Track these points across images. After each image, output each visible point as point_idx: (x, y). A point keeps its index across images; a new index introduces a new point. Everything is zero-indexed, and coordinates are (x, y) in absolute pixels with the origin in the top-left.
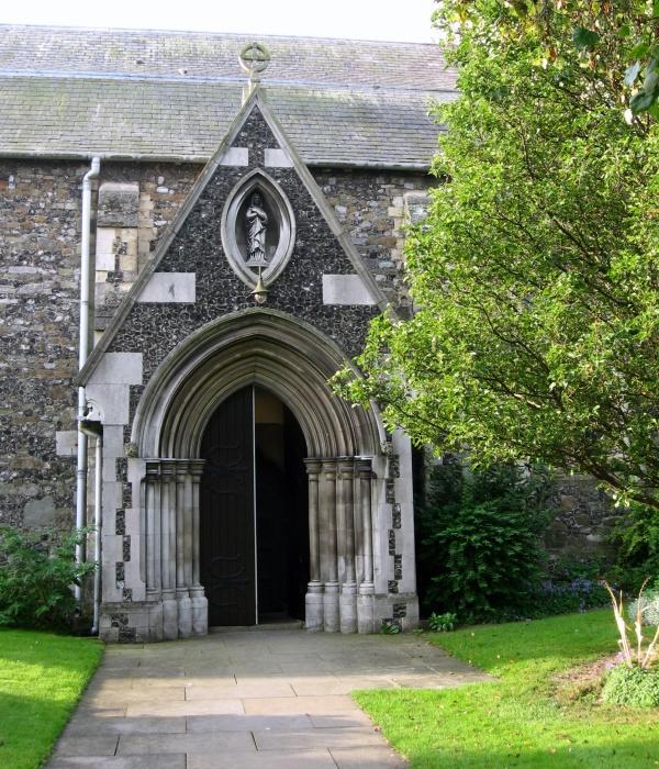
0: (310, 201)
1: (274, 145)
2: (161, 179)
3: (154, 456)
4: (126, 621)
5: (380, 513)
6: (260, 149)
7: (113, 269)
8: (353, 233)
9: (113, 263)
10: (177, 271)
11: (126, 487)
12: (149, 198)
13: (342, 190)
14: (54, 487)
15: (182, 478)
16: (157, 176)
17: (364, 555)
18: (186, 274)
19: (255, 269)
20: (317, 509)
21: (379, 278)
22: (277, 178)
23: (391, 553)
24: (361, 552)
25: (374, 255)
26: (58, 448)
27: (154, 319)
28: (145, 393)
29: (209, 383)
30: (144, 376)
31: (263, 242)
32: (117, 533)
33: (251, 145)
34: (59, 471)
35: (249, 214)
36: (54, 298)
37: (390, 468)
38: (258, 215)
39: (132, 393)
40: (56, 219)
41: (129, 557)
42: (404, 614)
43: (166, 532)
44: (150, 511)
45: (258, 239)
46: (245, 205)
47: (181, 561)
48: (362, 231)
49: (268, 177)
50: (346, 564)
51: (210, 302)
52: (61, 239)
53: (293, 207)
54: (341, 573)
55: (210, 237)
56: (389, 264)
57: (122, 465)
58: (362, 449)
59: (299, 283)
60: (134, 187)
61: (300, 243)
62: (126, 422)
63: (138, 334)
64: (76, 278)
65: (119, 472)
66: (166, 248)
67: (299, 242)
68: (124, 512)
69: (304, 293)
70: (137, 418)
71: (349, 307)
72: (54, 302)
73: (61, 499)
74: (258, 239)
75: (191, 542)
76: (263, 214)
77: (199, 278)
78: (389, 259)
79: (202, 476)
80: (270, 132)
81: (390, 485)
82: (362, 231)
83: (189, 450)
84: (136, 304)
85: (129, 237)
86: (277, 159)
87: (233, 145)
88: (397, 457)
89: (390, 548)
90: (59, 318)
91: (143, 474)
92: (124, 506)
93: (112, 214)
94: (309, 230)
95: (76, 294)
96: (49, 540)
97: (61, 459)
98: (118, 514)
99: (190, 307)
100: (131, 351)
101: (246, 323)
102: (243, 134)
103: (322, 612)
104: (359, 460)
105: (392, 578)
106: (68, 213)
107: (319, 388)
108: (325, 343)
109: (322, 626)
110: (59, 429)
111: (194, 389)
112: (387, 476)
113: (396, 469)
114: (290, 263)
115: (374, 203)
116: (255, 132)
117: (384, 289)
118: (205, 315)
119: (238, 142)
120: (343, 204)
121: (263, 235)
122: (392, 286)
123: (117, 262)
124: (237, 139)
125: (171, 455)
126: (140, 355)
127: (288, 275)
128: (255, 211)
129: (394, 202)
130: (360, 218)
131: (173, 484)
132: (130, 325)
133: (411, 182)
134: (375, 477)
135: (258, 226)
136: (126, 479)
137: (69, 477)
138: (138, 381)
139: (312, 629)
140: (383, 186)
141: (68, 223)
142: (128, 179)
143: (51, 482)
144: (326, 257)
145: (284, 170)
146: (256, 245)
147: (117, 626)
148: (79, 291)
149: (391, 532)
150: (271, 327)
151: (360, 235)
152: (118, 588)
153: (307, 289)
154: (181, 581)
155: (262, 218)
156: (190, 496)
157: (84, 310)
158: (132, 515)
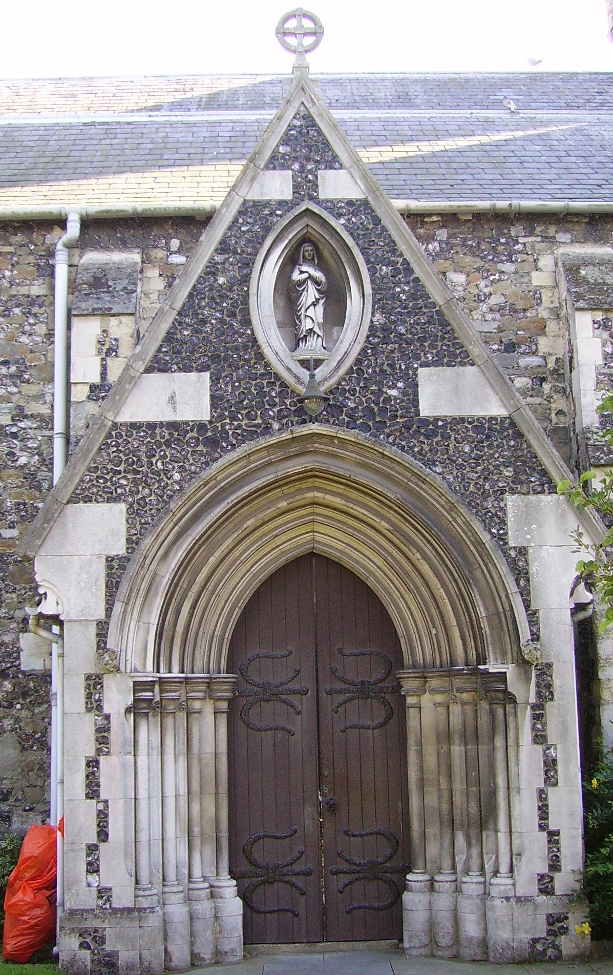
0: (394, 251)
1: (332, 163)
2: (175, 244)
3: (149, 674)
4: (102, 940)
5: (528, 757)
6: (310, 171)
7: (97, 379)
8: (476, 315)
9: (98, 370)
10: (180, 370)
11: (101, 721)
12: (156, 273)
13: (458, 249)
14: (17, 720)
15: (197, 705)
16: (168, 238)
17: (496, 831)
18: (193, 375)
19: (305, 363)
20: (420, 754)
21: (521, 382)
22: (339, 216)
23: (542, 827)
24: (491, 827)
25: (511, 347)
26: (22, 658)
27: (143, 449)
28: (132, 569)
29: (237, 552)
30: (129, 541)
31: (321, 320)
32: (88, 796)
33: (296, 166)
34: (25, 695)
35: (296, 276)
36: (14, 430)
37: (538, 685)
38: (310, 277)
39: (110, 567)
40: (17, 311)
41: (107, 835)
42: (565, 931)
43: (170, 792)
44: (142, 760)
45: (313, 314)
46: (291, 261)
47: (197, 842)
48: (491, 310)
49: (325, 214)
50: (469, 844)
51: (233, 418)
52: (24, 339)
53: (367, 261)
54: (460, 858)
55: (233, 315)
56: (534, 361)
57: (94, 683)
58: (491, 656)
59: (380, 383)
60: (135, 257)
61: (379, 319)
62: (101, 615)
63: (119, 472)
64: (48, 398)
65: (89, 696)
66: (162, 334)
67: (378, 316)
68: (97, 762)
69: (388, 399)
70: (118, 607)
71: (462, 420)
72: (14, 435)
73: (28, 737)
74: (313, 314)
75: (213, 809)
76: (318, 275)
77: (215, 380)
78: (534, 353)
79: (231, 702)
80: (327, 144)
81: (538, 716)
82: (491, 310)
83: (208, 655)
84: (115, 425)
85: (121, 329)
86: (337, 185)
87: (267, 167)
88: (549, 666)
89: (541, 818)
90: (23, 460)
91: (130, 701)
92: (99, 751)
93: (94, 291)
94: (395, 297)
95: (47, 422)
96: (12, 800)
97: (28, 675)
98: (88, 765)
99: (201, 427)
100: (109, 500)
101: (293, 450)
102: (282, 149)
103: (432, 926)
104: (486, 672)
105: (545, 870)
106: (33, 301)
107: (418, 556)
108: (424, 481)
109: (433, 941)
110: (24, 630)
111: (212, 560)
112: (533, 699)
113: (549, 686)
114: (364, 351)
115: (508, 267)
116: (307, 146)
117: (529, 399)
118: (226, 439)
119: (276, 162)
120: (458, 269)
121: (320, 308)
122: (540, 394)
123: (104, 368)
124: (273, 157)
125: (176, 668)
126: (120, 508)
127: (360, 371)
128: (305, 271)
129: (540, 264)
130: (487, 290)
131: (183, 715)
132: (131, 463)
133: (566, 231)
134: (513, 700)
135: (310, 294)
136: (100, 708)
137: (40, 704)
138: (119, 548)
139: (414, 952)
140: (521, 240)
141: (35, 315)
142: (124, 245)
143: (14, 712)
144: (421, 340)
145: (350, 203)
146: (307, 324)
147: (89, 948)
148: (52, 419)
149: (541, 792)
150: (335, 456)
151: (489, 317)
152: (89, 885)
153: (393, 393)
154: (197, 872)
155: (316, 282)
156: (211, 730)
157: (59, 444)
158: (111, 770)
